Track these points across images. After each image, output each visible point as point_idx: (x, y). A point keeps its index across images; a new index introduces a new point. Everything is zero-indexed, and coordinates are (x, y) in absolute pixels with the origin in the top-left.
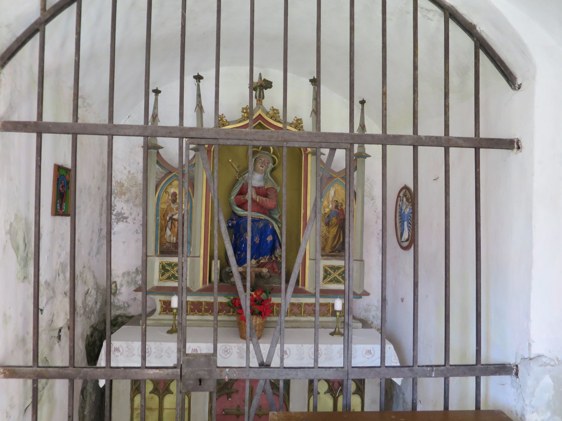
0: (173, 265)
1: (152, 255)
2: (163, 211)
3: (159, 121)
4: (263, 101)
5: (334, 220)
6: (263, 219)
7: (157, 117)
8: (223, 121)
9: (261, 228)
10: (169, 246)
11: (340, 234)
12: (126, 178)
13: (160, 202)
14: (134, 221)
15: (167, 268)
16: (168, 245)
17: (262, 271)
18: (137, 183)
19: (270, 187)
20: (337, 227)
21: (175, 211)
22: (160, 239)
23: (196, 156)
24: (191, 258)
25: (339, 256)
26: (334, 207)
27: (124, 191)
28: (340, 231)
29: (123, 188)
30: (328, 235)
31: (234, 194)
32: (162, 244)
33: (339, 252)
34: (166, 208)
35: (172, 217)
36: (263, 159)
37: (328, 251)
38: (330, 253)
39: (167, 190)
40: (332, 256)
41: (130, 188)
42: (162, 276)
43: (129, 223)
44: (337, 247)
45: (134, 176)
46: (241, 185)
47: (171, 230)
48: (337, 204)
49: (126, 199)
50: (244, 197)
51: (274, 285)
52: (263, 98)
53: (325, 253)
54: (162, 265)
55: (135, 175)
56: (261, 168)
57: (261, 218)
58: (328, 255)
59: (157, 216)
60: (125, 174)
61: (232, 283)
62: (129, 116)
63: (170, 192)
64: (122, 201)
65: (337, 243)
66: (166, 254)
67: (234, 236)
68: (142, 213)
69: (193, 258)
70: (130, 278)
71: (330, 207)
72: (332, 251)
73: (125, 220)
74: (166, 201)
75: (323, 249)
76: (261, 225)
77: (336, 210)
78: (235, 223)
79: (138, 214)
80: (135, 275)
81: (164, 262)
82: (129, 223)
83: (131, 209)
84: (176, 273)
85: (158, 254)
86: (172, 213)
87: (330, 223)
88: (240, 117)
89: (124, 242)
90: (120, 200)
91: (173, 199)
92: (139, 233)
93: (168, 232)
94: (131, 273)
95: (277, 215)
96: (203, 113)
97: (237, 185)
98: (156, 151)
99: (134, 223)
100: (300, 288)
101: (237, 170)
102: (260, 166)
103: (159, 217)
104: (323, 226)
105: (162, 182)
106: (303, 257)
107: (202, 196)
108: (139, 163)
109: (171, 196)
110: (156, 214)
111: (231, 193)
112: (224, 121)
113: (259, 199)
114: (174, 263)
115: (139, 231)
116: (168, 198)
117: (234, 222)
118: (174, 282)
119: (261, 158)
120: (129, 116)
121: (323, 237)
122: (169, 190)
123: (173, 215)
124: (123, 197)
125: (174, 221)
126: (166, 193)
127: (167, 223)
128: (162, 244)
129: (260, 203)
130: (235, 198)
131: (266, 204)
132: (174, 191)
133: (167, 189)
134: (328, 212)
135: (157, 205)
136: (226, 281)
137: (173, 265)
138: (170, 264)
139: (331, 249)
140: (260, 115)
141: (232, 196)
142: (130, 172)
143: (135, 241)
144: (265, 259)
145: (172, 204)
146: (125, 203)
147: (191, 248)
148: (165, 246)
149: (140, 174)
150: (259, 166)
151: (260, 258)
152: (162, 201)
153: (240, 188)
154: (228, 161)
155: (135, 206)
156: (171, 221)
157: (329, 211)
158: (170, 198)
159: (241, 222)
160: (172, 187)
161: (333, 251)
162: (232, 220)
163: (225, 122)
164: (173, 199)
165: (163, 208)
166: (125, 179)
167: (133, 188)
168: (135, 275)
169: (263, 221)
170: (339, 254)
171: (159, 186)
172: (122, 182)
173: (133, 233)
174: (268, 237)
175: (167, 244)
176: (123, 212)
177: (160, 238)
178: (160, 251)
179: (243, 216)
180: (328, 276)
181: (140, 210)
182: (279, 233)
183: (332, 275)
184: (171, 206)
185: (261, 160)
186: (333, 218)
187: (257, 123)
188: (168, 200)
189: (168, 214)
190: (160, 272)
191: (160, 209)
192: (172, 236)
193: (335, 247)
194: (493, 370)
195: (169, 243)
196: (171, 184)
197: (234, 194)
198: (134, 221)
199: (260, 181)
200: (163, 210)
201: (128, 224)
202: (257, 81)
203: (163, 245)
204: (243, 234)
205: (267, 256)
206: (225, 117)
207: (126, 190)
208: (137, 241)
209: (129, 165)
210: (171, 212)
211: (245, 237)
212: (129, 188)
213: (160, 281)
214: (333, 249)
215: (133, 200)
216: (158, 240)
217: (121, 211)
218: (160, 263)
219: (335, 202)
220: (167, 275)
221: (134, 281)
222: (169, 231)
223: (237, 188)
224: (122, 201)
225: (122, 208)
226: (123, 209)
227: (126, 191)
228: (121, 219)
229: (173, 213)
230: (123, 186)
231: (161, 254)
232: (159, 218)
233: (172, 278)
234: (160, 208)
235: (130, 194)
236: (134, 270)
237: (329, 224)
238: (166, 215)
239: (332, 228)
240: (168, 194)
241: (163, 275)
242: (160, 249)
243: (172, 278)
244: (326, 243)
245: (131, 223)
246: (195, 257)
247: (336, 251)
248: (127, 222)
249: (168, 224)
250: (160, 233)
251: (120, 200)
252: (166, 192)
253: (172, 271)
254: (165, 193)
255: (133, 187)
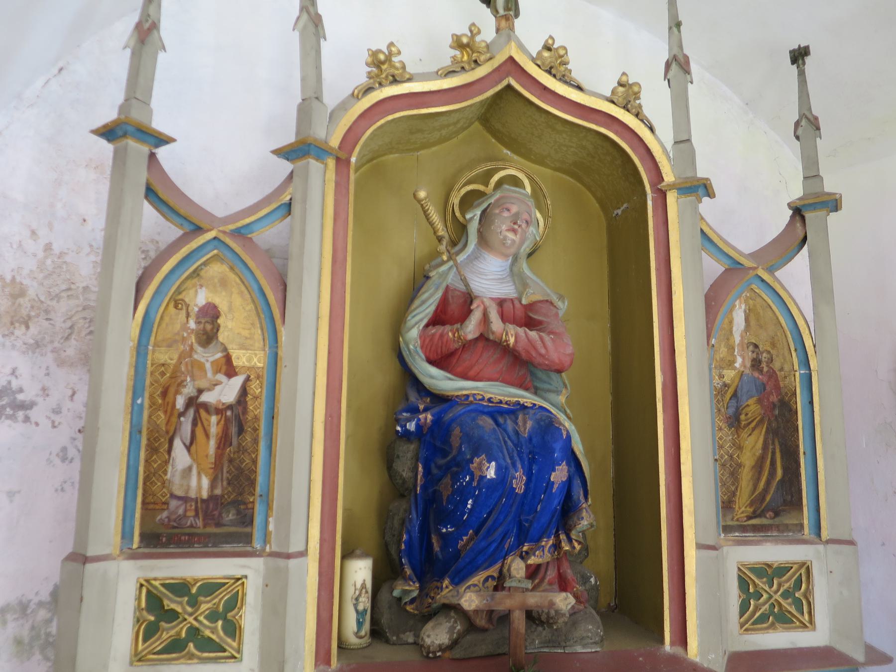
0: (194, 590)
1: (106, 551)
2: (163, 374)
3: (164, 48)
4: (517, 22)
5: (753, 408)
6: (526, 407)
7: (155, 32)
8: (392, 66)
9: (530, 439)
10: (181, 511)
11: (774, 453)
12: (34, 268)
13: (152, 339)
14: (53, 418)
15: (169, 604)
17: (552, 604)
18: (73, 286)
19: (541, 298)
20: (764, 430)
21: (210, 374)
22: (144, 484)
23: (295, 178)
24: (269, 559)
25: (778, 528)
26: (748, 364)
27: (24, 312)
28: (773, 444)
29: (21, 300)
30: (738, 456)
31: (416, 324)
32: (151, 506)
33: (777, 514)
34: (174, 362)
35: (198, 397)
36: (514, 209)
37: (742, 513)
38: (749, 518)
39: (180, 297)
40: (756, 529)
41: (49, 303)
42: (145, 640)
43: (37, 424)
44: (768, 499)
45: (65, 262)
46: (439, 294)
47: (193, 448)
48: (758, 354)
49: (32, 341)
50: (458, 330)
51: (579, 649)
52: (517, 15)
53: (732, 519)
54: (149, 592)
55: (68, 259)
56: (511, 235)
57: (522, 401)
58: (743, 529)
59: (136, 392)
60: (35, 255)
61: (428, 653)
62: (61, 70)
63: (192, 304)
64: (13, 347)
65: (768, 483)
66: (166, 545)
67: (424, 468)
68: (86, 387)
69: (281, 562)
70: (28, 626)
71: (737, 365)
72: (754, 512)
73: (21, 414)
74: (177, 337)
75: (727, 506)
76: (527, 426)
77: (756, 374)
78: (428, 421)
79: (70, 392)
80: (49, 615)
81: (155, 579)
82: (37, 424)
83: (48, 374)
84: (206, 622)
85: (135, 546)
86: (196, 383)
87: (743, 417)
88: (447, 62)
89: (11, 494)
90: (8, 343)
91: (204, 329)
92: (71, 461)
93: (180, 456)
94: (32, 606)
95: (558, 392)
96: (322, 40)
97: (424, 293)
98: (145, 149)
99: (56, 424)
100: (669, 654)
101: (441, 233)
102: (508, 230)
103: (147, 395)
104: (720, 429)
107: (318, 318)
108: (85, 220)
109: (197, 318)
110: (131, 383)
111: (405, 315)
112: (398, 65)
113: (517, 337)
114: (198, 584)
115: (72, 452)
116: (185, 327)
117: (426, 419)
118: (196, 661)
119: (508, 205)
120: (61, 70)
121: (723, 465)
122: (187, 296)
123: (200, 391)
124: (20, 331)
125: (203, 413)
126: (176, 307)
127: (174, 419)
128: (151, 506)
129: (520, 348)
130: (422, 335)
131: (543, 351)
132: (210, 300)
133: (184, 293)
134: (733, 380)
135: (141, 350)
136: (395, 638)
137: (194, 590)
138: (180, 588)
139: (751, 505)
140: (511, 59)
141: (413, 327)
142: (51, 249)
143: (56, 490)
144: (543, 551)
145: (199, 349)
146: (24, 353)
147: (271, 519)
148: (165, 514)
149: (88, 254)
150: (504, 227)
151: (525, 548)
152: (160, 338)
153: (437, 302)
154: (415, 196)
155: (61, 363)
156: (191, 412)
157: (735, 377)
158: (192, 324)
159: (450, 416)
160: (201, 286)
161: (759, 512)
162: (415, 411)
163: (397, 69)
164: (204, 329)
165: (163, 365)
166: (31, 271)
167: (58, 302)
168: (49, 615)
169: (532, 412)
170: (777, 521)
171: (152, 278)
172: (18, 279)
173: (49, 461)
174: (554, 470)
175: (174, 503)
176: (15, 384)
179: (457, 396)
180: (752, 602)
181: (80, 379)
182: (581, 452)
183: (765, 596)
184: (195, 356)
185: (508, 210)
186: (751, 402)
187: (499, 87)
188: (185, 335)
189: (181, 384)
190: (138, 621)
191: (149, 369)
192: (194, 471)
193: (764, 499)
194: (573, 589)
195: (180, 502)
196: (196, 273)
197: (416, 324)
198: (53, 417)
199: (501, 280)
200: (163, 369)
201: (34, 426)
203: (157, 507)
204: (471, 461)
205: (549, 537)
206: (399, 53)
207: (32, 307)
208: (62, 490)
209: (50, 226)
210: (193, 379)
211: (477, 474)
212: (42, 302)
213: (140, 660)
214: (759, 507)
215: (56, 344)
216: (136, 488)
217: (9, 382)
218: (142, 585)
219: (751, 348)
220: (167, 633)
221: (43, 637)
222: (185, 452)
223: (431, 301)
224: (13, 346)
225: (13, 372)
226: (17, 373)
227: (33, 314)
228: (8, 409)
229: (202, 384)
230: (22, 293)
231: (147, 546)
232: (144, 401)
233: (191, 645)
234: (152, 365)
235: (46, 324)
236: (45, 596)
237: (738, 420)
238: (172, 390)
239: (750, 435)
240: (184, 312)
241: (151, 631)
243: (191, 645)
244: (733, 484)
245: (45, 424)
246: (289, 556)
247: (768, 511)
248: (27, 419)
249: (179, 423)
250: (146, 461)
251: (8, 343)
252: (177, 303)
253: (191, 615)
254: (172, 305)
255: (58, 297)
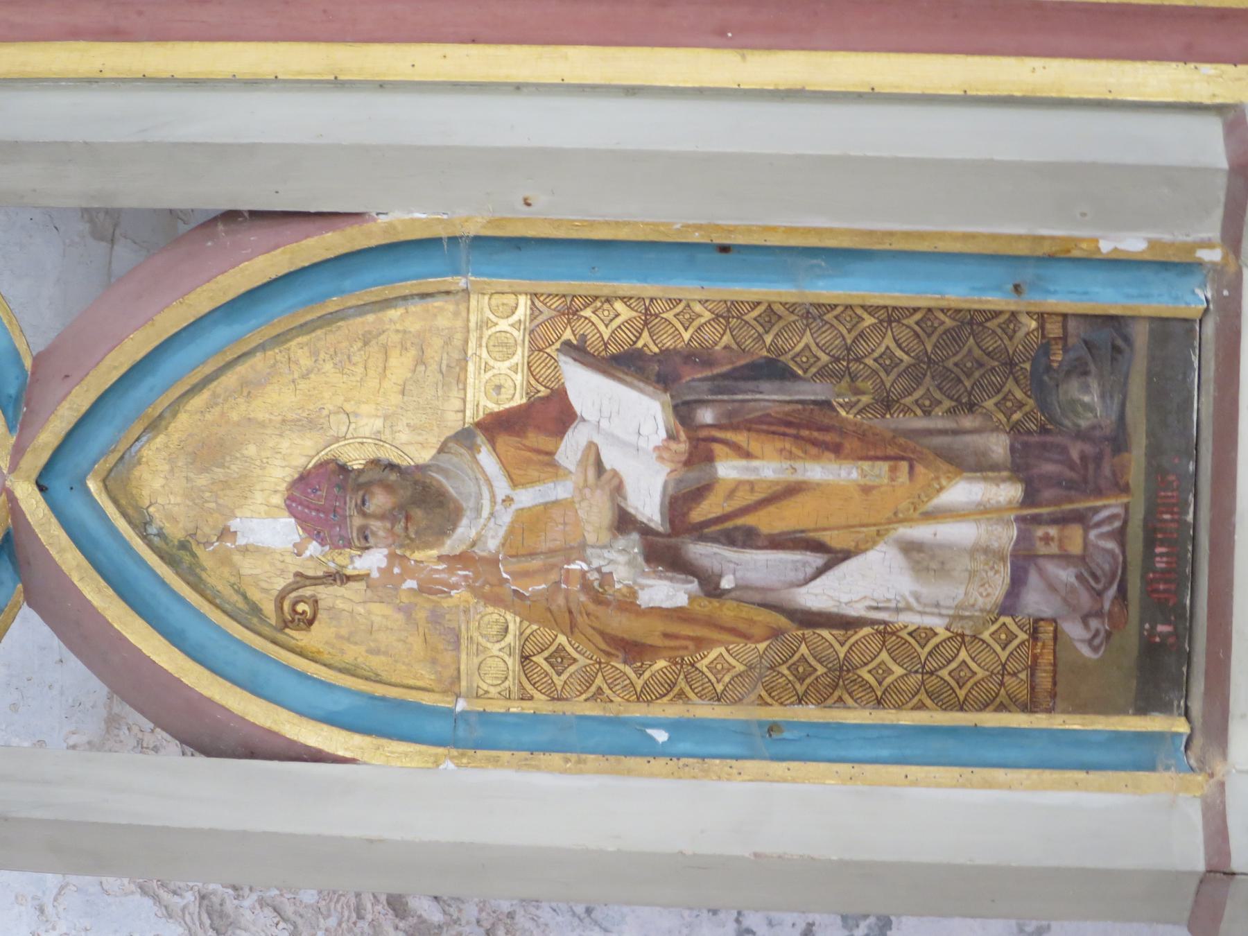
2: (559, 659)
13: (427, 699)
16: (1052, 587)
21: (561, 491)
34: (513, 622)
35: (645, 531)
39: (269, 608)
47: (834, 539)
63: (294, 565)
66: (1183, 619)
86: (591, 538)
103: (638, 711)
105: (172, 683)
106: (320, 751)
123: (624, 522)
127: (728, 612)
145: (465, 531)
147: (1106, 247)
148: (1074, 630)
152: (426, 676)
156: (702, 552)
158: (373, 561)
160: (225, 533)
165: (525, 658)
171: (198, 704)
175: (1036, 601)
177: (946, 707)
178: (1143, 707)
184: (493, 544)
191: (541, 704)
192: (921, 532)
195: (1033, 578)
202: (556, 457)
210: (580, 550)
238: (620, 624)
242: (1120, 711)
250: (879, 703)
254: (300, 638)
